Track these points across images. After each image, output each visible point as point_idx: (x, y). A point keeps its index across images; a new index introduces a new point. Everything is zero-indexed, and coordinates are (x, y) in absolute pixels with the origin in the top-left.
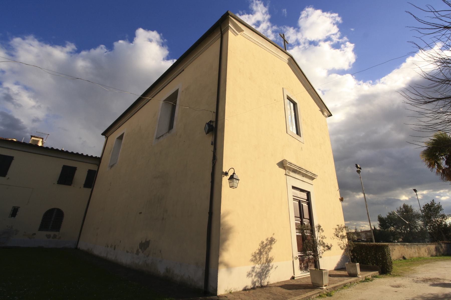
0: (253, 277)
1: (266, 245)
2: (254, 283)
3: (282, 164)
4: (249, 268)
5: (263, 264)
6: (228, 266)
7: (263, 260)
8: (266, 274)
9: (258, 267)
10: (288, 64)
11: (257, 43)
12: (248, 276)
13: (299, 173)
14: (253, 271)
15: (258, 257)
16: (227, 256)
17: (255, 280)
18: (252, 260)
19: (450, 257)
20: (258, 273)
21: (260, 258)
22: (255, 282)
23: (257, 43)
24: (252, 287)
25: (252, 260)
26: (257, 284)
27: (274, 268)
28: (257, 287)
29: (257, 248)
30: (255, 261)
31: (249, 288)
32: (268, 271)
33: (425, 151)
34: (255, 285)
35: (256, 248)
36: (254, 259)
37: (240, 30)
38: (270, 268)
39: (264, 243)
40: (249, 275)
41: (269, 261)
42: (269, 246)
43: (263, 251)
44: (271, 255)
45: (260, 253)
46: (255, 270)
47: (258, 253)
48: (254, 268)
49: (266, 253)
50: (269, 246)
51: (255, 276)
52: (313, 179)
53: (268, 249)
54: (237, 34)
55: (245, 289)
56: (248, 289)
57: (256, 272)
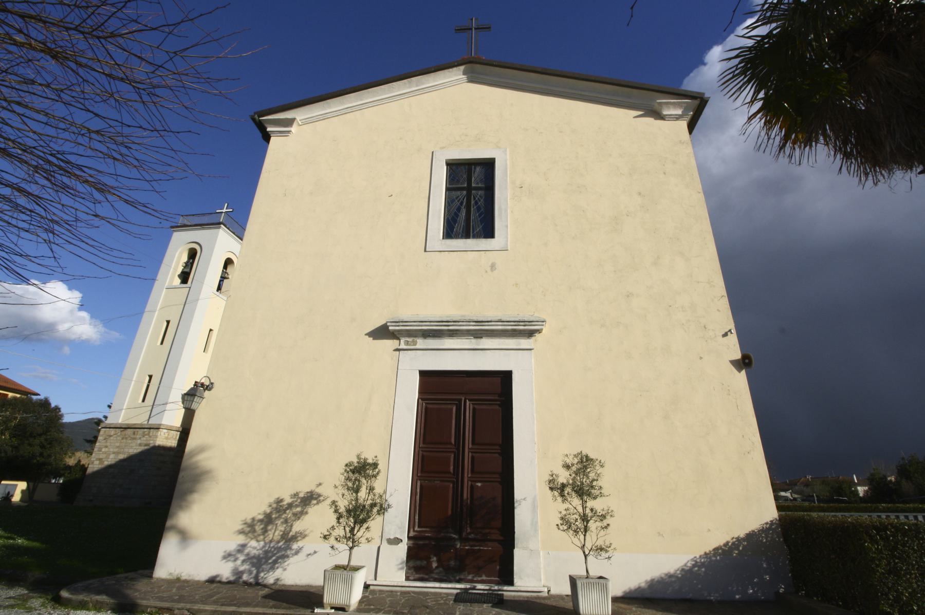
0: (239, 562)
1: (290, 506)
2: (238, 573)
3: (382, 332)
4: (232, 545)
5: (271, 542)
6: (185, 536)
7: (275, 533)
8: (275, 562)
9: (255, 546)
10: (471, 80)
11: (349, 110)
12: (225, 558)
13: (453, 334)
14: (239, 551)
15: (259, 528)
16: (187, 517)
17: (242, 568)
18: (241, 532)
19: (5, 373)
20: (254, 557)
21: (265, 531)
22: (242, 573)
23: (343, 112)
24: (232, 578)
25: (241, 532)
26: (245, 577)
27: (302, 555)
28: (246, 583)
29: (262, 510)
30: (250, 535)
31: (224, 580)
32: (285, 557)
33: (750, 49)
34: (240, 577)
35: (258, 508)
36: (248, 529)
37: (290, 122)
38: (289, 552)
39: (285, 503)
40: (228, 556)
41: (289, 539)
42: (299, 509)
43: (279, 517)
44: (298, 527)
45: (268, 520)
46: (246, 551)
47: (261, 521)
48: (244, 546)
49: (286, 521)
50: (299, 509)
51: (244, 561)
52: (530, 334)
53: (295, 515)
54: (289, 132)
55: (212, 580)
56: (220, 582)
57: (248, 554)
